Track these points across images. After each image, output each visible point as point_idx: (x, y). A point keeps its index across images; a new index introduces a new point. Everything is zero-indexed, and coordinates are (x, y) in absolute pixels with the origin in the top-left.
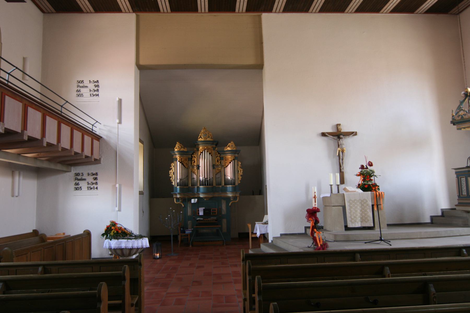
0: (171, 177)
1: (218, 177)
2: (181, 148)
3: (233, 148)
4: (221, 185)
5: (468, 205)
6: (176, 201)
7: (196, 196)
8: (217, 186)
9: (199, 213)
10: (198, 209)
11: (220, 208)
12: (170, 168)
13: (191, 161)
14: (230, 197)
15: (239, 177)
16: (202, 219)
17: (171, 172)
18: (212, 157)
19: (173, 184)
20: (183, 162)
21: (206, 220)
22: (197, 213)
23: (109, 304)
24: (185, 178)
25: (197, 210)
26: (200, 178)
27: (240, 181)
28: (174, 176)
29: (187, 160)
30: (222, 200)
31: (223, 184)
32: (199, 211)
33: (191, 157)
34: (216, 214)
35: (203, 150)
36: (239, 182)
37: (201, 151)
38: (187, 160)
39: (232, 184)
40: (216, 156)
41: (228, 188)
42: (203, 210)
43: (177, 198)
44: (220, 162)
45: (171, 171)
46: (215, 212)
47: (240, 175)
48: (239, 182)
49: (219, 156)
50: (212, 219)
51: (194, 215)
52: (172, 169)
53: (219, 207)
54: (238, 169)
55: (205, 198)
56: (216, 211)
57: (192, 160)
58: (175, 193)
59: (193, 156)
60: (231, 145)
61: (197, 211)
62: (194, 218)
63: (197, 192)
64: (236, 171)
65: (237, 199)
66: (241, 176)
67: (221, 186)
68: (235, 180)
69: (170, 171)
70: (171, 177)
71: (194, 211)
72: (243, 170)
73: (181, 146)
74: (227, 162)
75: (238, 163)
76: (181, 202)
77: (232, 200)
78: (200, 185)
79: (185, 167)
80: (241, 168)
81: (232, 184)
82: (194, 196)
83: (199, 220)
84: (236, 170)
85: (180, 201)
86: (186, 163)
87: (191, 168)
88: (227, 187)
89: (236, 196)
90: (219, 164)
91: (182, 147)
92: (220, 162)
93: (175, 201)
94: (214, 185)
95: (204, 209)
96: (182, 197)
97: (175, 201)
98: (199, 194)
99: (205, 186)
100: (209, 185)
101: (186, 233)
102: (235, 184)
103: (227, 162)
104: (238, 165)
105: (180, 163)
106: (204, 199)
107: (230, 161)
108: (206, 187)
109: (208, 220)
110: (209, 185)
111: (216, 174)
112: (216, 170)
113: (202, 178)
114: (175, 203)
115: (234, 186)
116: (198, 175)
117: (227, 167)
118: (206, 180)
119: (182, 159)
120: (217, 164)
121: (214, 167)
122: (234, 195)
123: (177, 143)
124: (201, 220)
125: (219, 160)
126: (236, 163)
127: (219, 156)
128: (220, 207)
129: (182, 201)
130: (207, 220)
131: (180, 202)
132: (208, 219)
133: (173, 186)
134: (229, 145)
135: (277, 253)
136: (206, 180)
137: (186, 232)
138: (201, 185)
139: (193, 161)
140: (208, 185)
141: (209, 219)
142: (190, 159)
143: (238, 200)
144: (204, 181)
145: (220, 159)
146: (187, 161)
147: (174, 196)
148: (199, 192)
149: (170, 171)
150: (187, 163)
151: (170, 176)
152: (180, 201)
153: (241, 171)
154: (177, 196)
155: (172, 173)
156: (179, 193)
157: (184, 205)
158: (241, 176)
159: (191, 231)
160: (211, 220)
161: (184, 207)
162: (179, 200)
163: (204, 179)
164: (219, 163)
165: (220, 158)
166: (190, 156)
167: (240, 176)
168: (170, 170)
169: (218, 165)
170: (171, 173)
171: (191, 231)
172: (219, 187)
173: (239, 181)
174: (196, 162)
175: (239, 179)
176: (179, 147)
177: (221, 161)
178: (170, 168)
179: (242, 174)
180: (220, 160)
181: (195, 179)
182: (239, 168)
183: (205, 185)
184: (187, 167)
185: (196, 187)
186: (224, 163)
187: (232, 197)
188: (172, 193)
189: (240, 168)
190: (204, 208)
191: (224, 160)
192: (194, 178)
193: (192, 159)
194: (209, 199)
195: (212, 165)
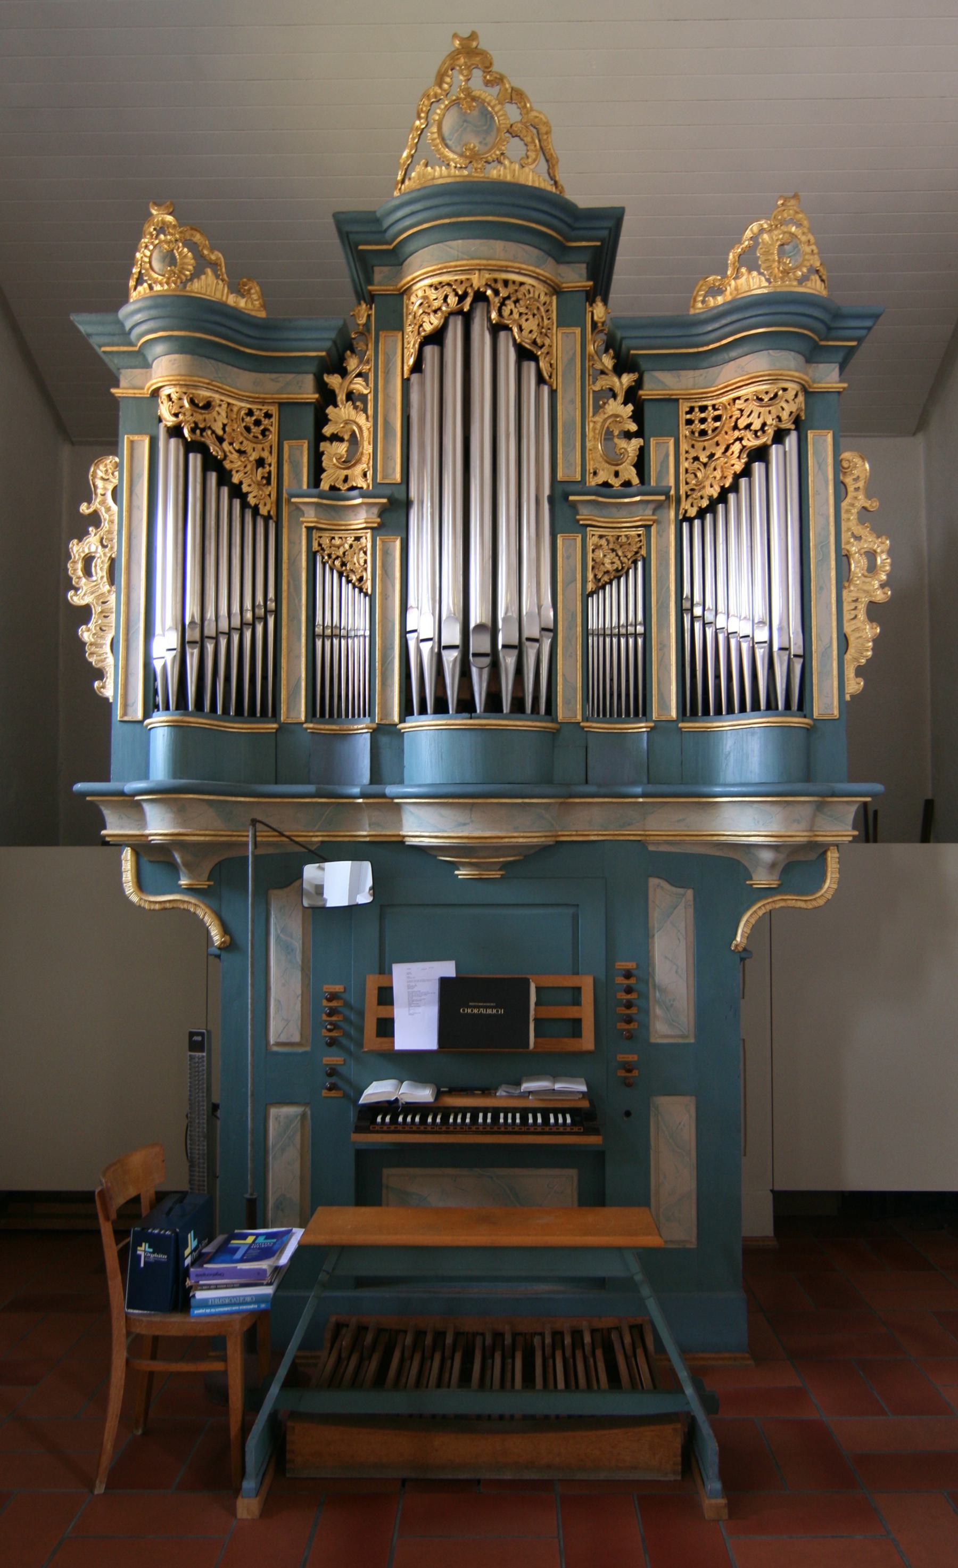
0: (84, 614)
1: (611, 621)
2: (198, 273)
3: (802, 281)
4: (641, 709)
5: (207, 726)
6: (140, 885)
7: (364, 832)
8: (597, 726)
9: (386, 1027)
10: (385, 971)
11: (628, 975)
12: (84, 509)
13: (320, 438)
14: (749, 848)
15: (848, 628)
16: (424, 1094)
17: (88, 561)
18: (553, 393)
19: (109, 692)
20: (220, 440)
21: (464, 1111)
22: (370, 1027)
23: (93, 1193)
24: (241, 631)
25: (373, 983)
26: (404, 632)
27: (860, 672)
28: (112, 599)
29: (264, 433)
30: (653, 881)
31: (664, 705)
32: (386, 996)
33: (313, 396)
34: (587, 1042)
35: (452, 300)
36: (854, 685)
37: (431, 323)
38: (273, 425)
39: (795, 705)
40: (598, 395)
41: (729, 744)
42: (432, 991)
43: (142, 848)
44: (641, 465)
45: (91, 543)
46: (571, 1012)
47: (865, 600)
48: (854, 685)
49: (631, 396)
50: (532, 1102)
51: (332, 1043)
52: (95, 519)
53: (622, 965)
54: (845, 536)
55: (465, 850)
56: (587, 1012)
57: (328, 430)
58: (122, 794)
59: (334, 380)
60: (778, 235)
61: (372, 996)
62: (332, 1072)
63: (372, 782)
64: (824, 559)
65: (823, 880)
66: (875, 611)
67: (642, 727)
68: (806, 656)
69: (77, 549)
70: (84, 614)
71: (333, 997)
72: (890, 553)
73: (192, 246)
74: (719, 452)
75: (838, 464)
76: (190, 890)
77: (762, 879)
78: (407, 711)
79: (245, 505)
80: (878, 533)
81: (771, 705)
82: (343, 834)
83: (391, 1107)
84: (823, 545)
85: (184, 882)
86: (260, 463)
87: (310, 517)
88: (718, 734)
89: (811, 846)
90: (627, 484)
91: (214, 265)
92: (641, 465)
93: (128, 877)
94: (561, 713)
95: (444, 983)
96: (197, 834)
97: (128, 877)
98: (394, 808)
99: (462, 721)
100: (506, 706)
101: (205, 1304)
102: (803, 706)
103: (719, 452)
104: (841, 490)
105: (190, 447)
106: (455, 865)
107: (752, 442)
108: (482, 730)
109: (496, 1112)
110: (506, 706)
111: (591, 594)
112: (592, 541)
113: (427, 630)
114: (126, 899)
115: (796, 721)
116: (385, 597)
117: (711, 508)
118: (480, 643)
119: (208, 406)
120: (606, 485)
121: (574, 506)
122: (799, 835)
123: (154, 212)
124: (412, 1108)
125: (628, 435)
126: (821, 465)
127: (631, 396)
128: (631, 965)
129: (203, 884)
130: (475, 1112)
131: (178, 890)
132: (487, 1091)
133: (105, 706)
134: (754, 238)
135: (183, 445)
136: (480, 643)
137: (200, 1295)
138: (423, 711)
139: (336, 438)
140: (494, 703)
141: (502, 1097)
142: (309, 418)
143: (830, 884)
144: (450, 657)
145: (633, 427)
146: (273, 437)
147: (115, 827)
148: (390, 790)
149: (77, 549)
150: (272, 460)
151: (77, 599)
152: (184, 882)
153: (871, 555)
154: (142, 820)
155: (100, 570)
156: (162, 794)
157: (225, 929)
158: (875, 611)
159: (268, 1290)
160: (524, 1112)
161: (231, 946)
162: (173, 867)
163: (452, 635)
164: (630, 473)
165: (637, 417)
166: (309, 380)
167: (862, 616)
168: (81, 535)
169: (616, 483)
170: (88, 572)
171: (268, 1290)
172: (622, 735)
173: (850, 672)
174: (367, 448)
175: (852, 651)
176: (170, 259)
177: (653, 441)
178: (84, 509)
179: (880, 596)
180: (639, 434)
181: (358, 648)
182: (851, 521)
183: (466, 706)
184: (263, 511)
185: (362, 728)
186: (685, 464)
187: (767, 856)
188: (79, 786)
189: (864, 532)
190: (448, 969)
191: (684, 431)
192: (336, 634)
193: (322, 420)
194: (505, 866)
195: (547, 491)
